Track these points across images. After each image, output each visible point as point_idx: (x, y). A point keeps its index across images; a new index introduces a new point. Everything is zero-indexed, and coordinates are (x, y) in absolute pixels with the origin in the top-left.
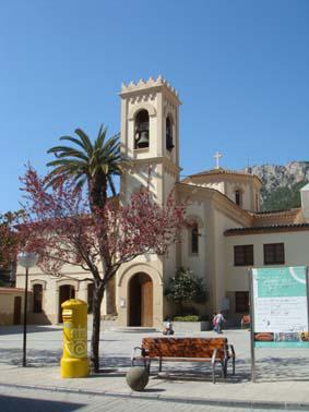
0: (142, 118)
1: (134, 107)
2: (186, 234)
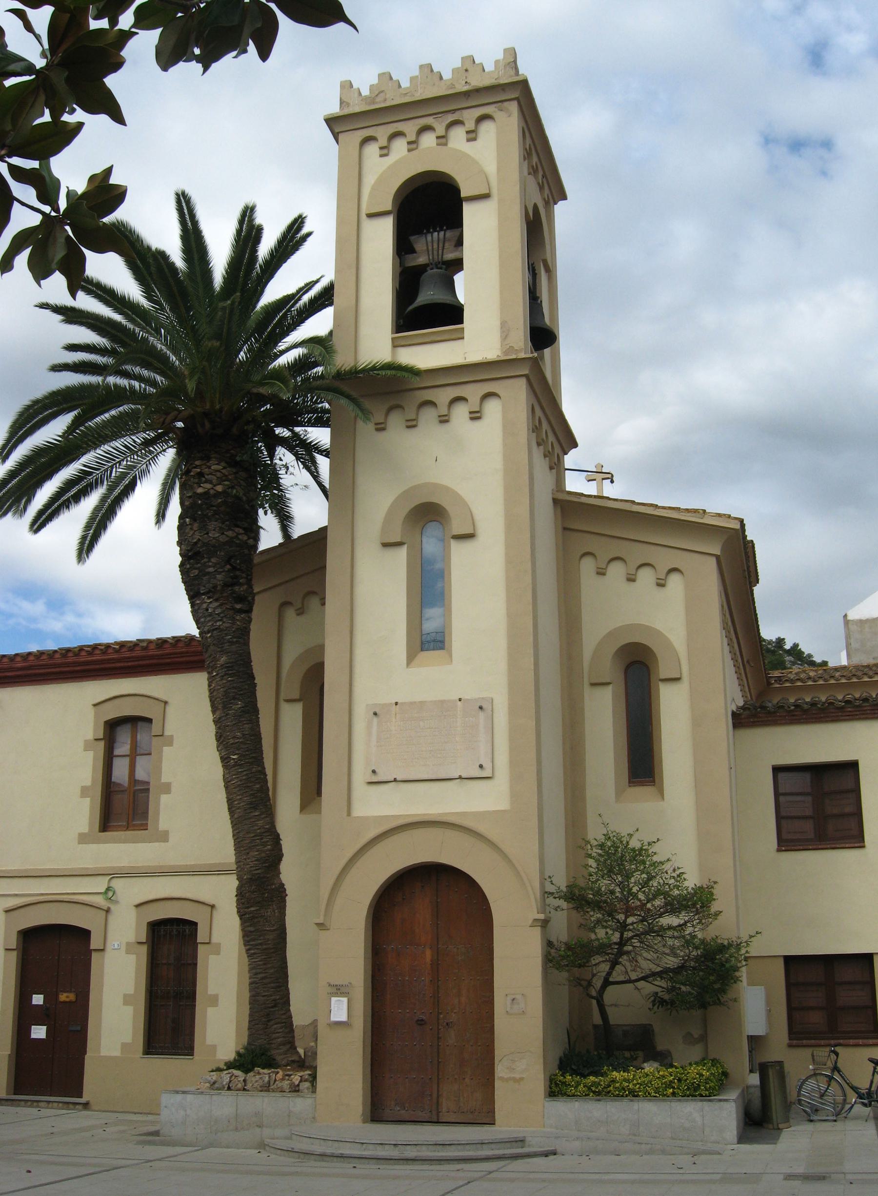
0: (428, 210)
1: (390, 167)
2: (603, 714)
